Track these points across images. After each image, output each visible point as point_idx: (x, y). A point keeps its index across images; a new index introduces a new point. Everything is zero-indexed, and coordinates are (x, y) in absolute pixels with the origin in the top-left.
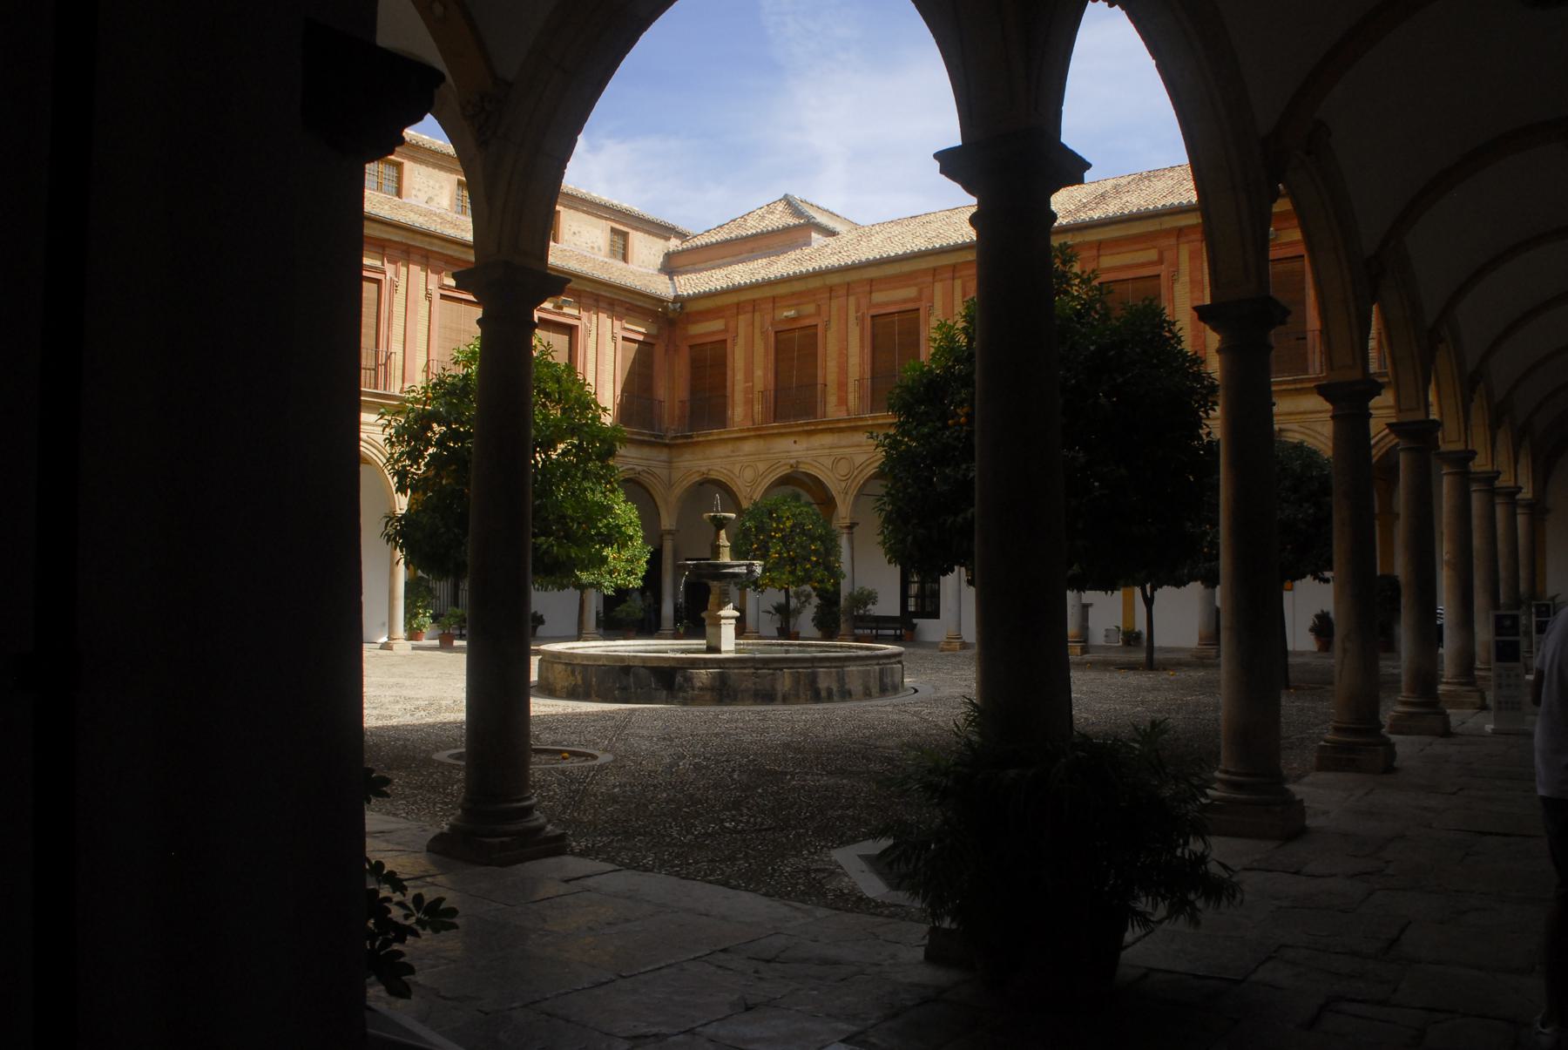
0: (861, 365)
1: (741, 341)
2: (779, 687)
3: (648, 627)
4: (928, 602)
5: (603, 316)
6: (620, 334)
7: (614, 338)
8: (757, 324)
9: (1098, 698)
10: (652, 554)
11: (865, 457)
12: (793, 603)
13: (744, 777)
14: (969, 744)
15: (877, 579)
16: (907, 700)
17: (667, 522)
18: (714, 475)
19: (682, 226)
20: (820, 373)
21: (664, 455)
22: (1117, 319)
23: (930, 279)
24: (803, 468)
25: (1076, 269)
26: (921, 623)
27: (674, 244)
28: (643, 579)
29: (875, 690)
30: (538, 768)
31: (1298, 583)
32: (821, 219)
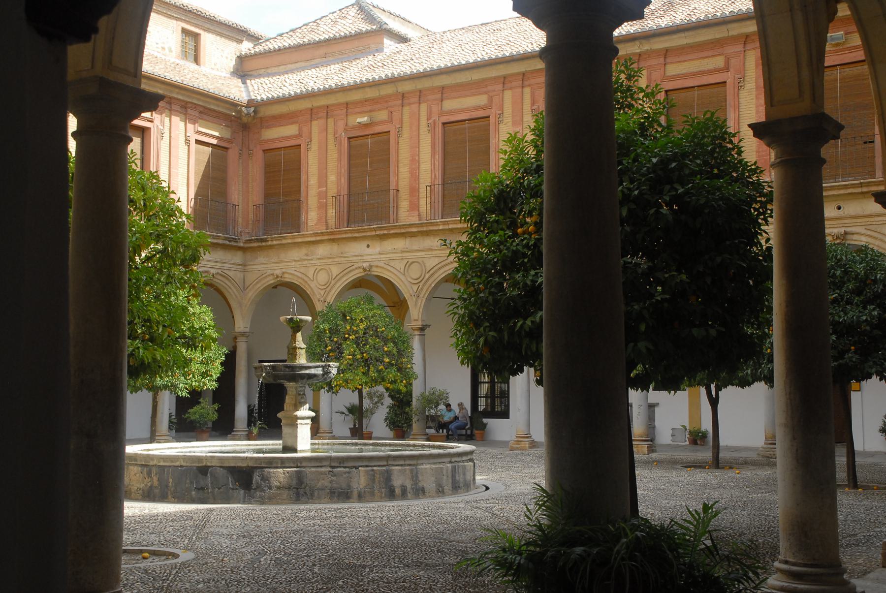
0: (433, 170)
1: (314, 146)
2: (354, 485)
3: (223, 428)
4: (497, 401)
5: (176, 119)
6: (193, 137)
7: (187, 142)
8: (331, 130)
9: (662, 494)
10: (227, 356)
11: (437, 261)
12: (367, 403)
13: (325, 571)
14: (540, 527)
15: (445, 376)
16: (479, 496)
17: (241, 324)
18: (288, 278)
19: (254, 27)
20: (392, 179)
21: (238, 258)
22: (679, 132)
23: (500, 87)
24: (376, 272)
25: (643, 83)
26: (493, 424)
27: (247, 47)
28: (218, 380)
29: (447, 488)
30: (126, 564)
31: (863, 383)
32: (394, 25)
